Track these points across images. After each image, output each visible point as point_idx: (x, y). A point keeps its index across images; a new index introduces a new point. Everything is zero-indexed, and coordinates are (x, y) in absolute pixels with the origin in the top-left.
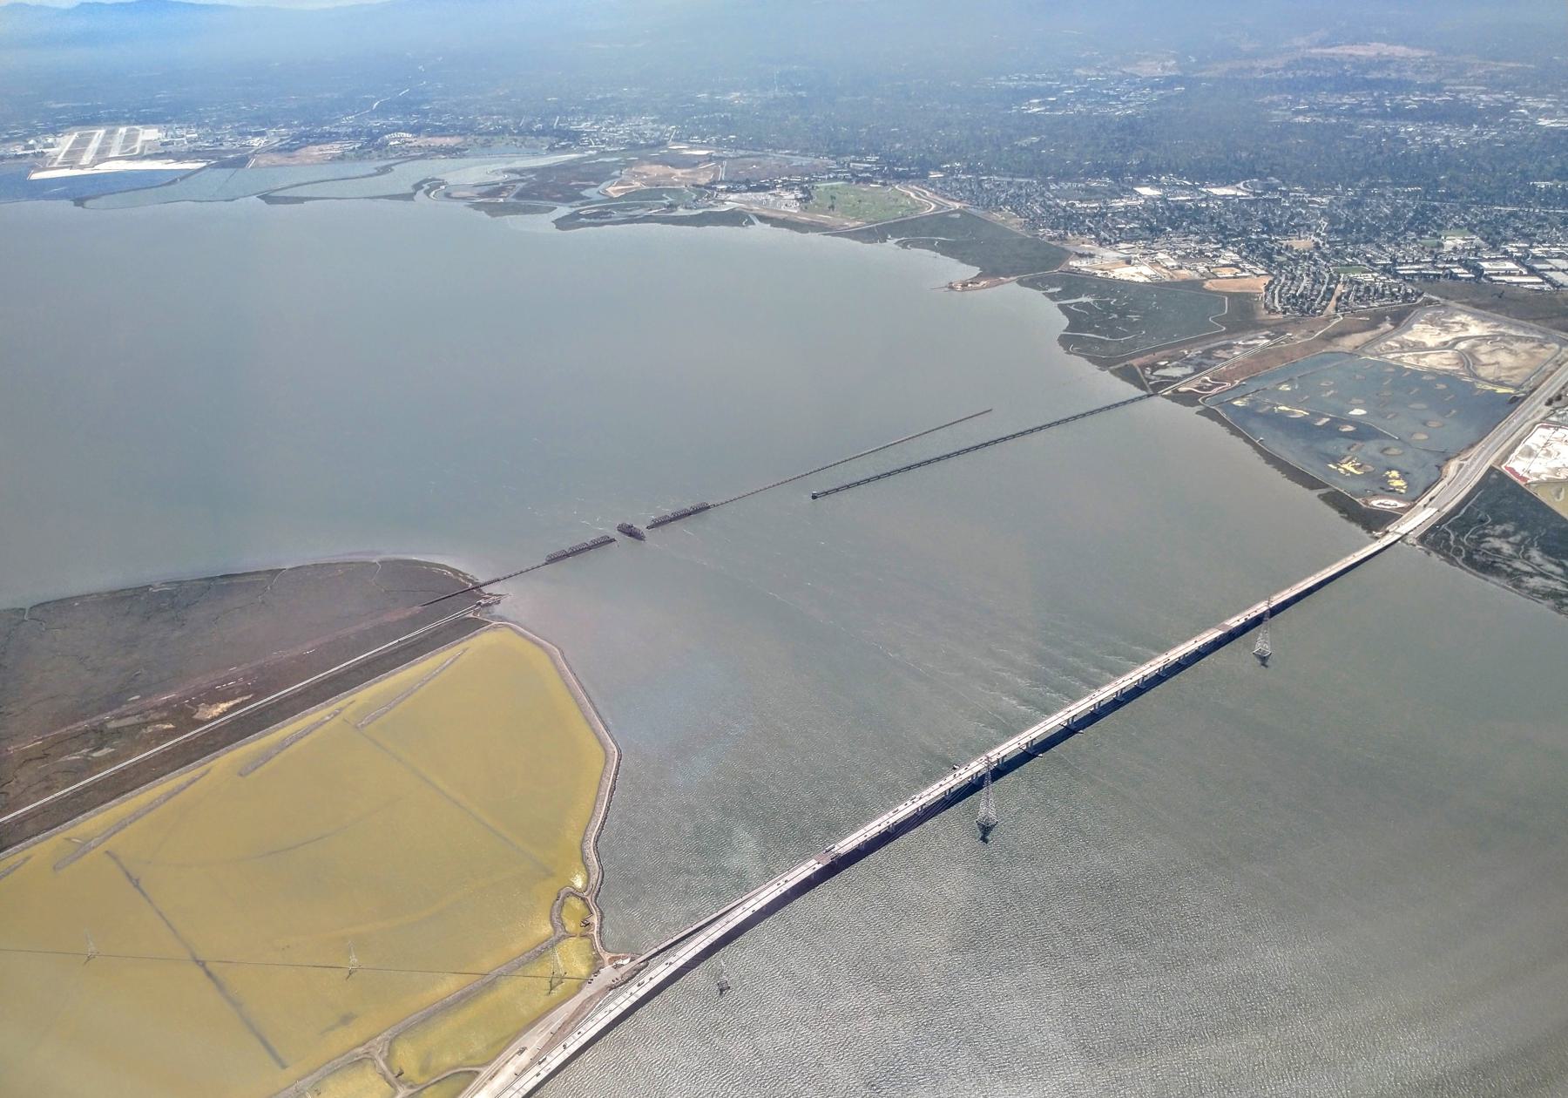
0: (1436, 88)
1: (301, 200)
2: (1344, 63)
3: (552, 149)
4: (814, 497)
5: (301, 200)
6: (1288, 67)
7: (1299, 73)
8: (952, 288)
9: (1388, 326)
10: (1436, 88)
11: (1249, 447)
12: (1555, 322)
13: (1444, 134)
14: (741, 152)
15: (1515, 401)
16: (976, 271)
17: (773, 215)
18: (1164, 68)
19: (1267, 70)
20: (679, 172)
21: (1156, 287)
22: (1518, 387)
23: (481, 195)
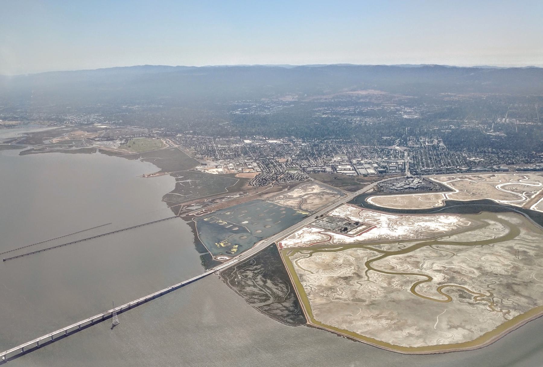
0: (378, 105)
1: (356, 341)
2: (353, 97)
3: (49, 126)
4: (4, 260)
5: (356, 341)
6: (333, 98)
7: (336, 100)
8: (144, 176)
9: (286, 190)
10: (378, 105)
11: (192, 235)
12: (346, 187)
13: (369, 121)
14: (118, 127)
15: (307, 216)
16: (160, 169)
17: (107, 150)
18: (293, 98)
19: (326, 99)
20: (367, 120)
21: (220, 175)
22: (310, 212)
23: (4, 143)
